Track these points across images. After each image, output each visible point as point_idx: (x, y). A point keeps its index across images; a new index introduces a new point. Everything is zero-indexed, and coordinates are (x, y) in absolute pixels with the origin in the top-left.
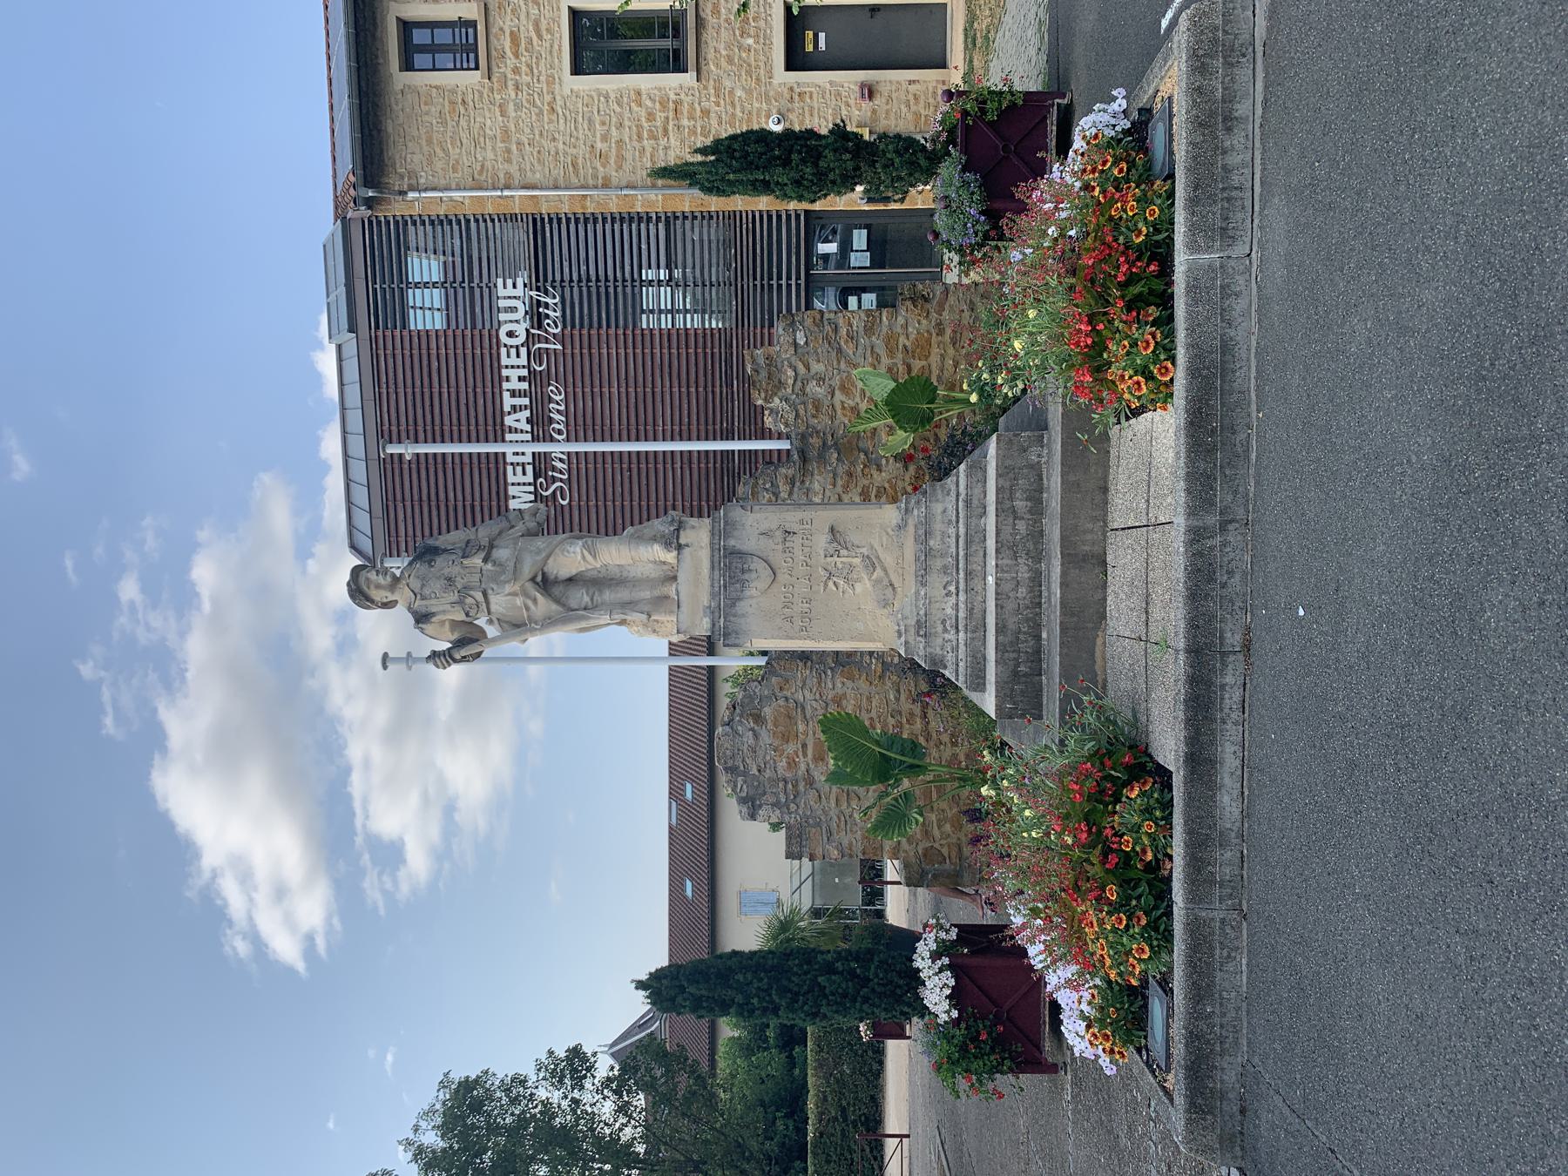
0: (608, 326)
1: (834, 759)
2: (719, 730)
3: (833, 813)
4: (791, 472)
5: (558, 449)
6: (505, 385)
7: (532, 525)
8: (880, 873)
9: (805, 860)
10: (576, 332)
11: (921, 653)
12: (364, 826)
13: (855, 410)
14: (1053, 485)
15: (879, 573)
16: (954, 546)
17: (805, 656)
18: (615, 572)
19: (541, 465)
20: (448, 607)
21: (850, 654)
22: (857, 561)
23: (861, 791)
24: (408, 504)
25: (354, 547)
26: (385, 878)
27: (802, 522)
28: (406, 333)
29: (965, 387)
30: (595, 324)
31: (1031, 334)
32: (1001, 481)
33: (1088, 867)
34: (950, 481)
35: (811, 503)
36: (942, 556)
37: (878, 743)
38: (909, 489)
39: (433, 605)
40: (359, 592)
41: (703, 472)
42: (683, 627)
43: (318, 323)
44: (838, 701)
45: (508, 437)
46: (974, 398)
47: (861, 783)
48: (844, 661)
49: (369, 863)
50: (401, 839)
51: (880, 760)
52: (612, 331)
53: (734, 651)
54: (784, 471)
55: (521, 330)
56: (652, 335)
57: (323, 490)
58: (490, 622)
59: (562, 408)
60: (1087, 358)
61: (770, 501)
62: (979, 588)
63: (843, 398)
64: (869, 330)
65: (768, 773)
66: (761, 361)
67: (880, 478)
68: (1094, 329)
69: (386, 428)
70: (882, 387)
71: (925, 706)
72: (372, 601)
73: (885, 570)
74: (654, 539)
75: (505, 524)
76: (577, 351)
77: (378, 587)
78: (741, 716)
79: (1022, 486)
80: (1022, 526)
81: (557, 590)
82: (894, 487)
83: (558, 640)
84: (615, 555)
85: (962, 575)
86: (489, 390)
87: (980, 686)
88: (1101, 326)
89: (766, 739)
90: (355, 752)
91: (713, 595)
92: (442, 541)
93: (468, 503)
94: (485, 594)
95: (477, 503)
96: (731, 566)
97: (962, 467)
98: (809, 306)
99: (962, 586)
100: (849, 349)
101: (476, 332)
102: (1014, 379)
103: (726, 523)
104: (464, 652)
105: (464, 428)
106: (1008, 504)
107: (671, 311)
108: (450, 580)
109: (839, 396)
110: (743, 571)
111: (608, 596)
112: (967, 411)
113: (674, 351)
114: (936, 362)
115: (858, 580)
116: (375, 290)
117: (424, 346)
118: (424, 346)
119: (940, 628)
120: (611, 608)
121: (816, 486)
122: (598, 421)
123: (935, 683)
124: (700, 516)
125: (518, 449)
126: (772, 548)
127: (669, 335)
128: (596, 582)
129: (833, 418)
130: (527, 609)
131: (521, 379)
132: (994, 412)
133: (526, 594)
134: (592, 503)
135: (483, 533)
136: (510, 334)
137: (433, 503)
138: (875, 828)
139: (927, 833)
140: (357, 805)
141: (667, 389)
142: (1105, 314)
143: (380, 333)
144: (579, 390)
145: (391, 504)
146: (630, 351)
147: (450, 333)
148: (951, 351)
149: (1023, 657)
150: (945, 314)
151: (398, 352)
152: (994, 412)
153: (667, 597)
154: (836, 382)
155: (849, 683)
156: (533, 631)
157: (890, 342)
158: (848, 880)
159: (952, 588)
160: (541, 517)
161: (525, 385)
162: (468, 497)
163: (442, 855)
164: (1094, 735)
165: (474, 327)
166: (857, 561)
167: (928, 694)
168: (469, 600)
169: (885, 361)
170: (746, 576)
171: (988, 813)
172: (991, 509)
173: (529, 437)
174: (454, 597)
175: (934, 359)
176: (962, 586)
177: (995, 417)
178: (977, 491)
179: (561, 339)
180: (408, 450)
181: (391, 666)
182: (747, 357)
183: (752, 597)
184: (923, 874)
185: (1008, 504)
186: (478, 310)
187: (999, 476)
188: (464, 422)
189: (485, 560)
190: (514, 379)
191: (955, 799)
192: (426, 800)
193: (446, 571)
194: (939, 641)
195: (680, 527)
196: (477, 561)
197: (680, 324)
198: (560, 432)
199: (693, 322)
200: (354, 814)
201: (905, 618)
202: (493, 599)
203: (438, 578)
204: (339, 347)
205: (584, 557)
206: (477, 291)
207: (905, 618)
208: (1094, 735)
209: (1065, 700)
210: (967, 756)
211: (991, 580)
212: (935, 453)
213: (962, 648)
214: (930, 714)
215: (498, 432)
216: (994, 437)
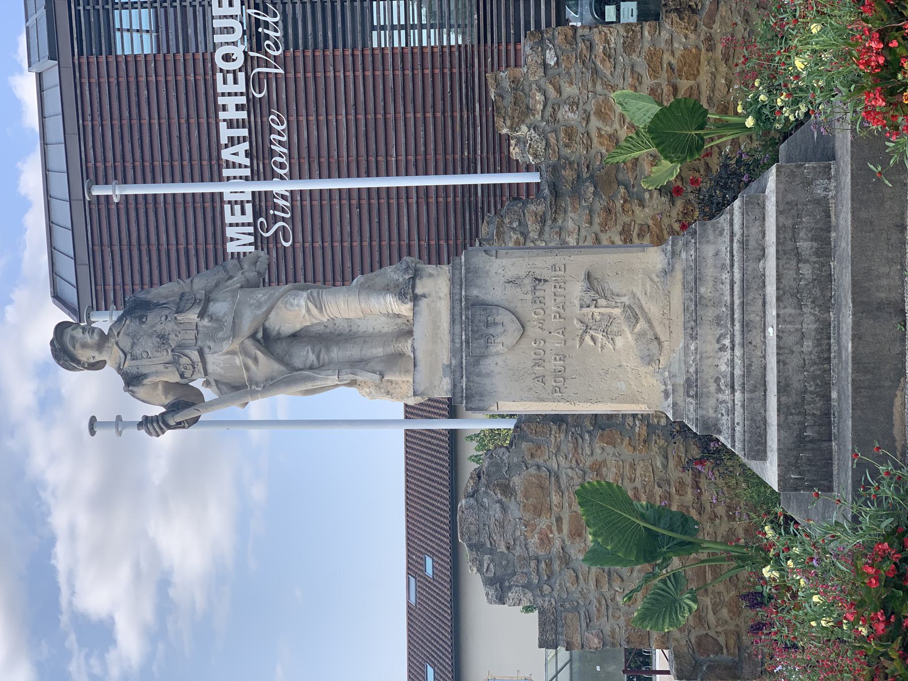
0: (335, 47)
1: (594, 534)
2: (463, 502)
3: (593, 596)
4: (540, 209)
5: (279, 187)
6: (222, 115)
7: (252, 275)
8: (647, 660)
9: (562, 650)
10: (299, 54)
11: (692, 416)
12: (70, 603)
13: (613, 138)
14: (842, 222)
15: (642, 325)
16: (728, 292)
17: (559, 420)
18: (343, 327)
19: (262, 204)
20: (161, 367)
21: (610, 417)
22: (617, 311)
23: (625, 571)
24: (116, 248)
25: (57, 297)
26: (94, 661)
27: (554, 267)
28: (112, 59)
29: (740, 109)
30: (321, 45)
31: (814, 52)
32: (781, 219)
33: (887, 663)
34: (723, 220)
35: (563, 246)
36: (714, 305)
37: (643, 517)
38: (677, 226)
39: (144, 366)
40: (64, 350)
41: (442, 207)
42: (421, 388)
43: (16, 45)
44: (597, 468)
45: (226, 172)
46: (750, 122)
47: (621, 562)
48: (603, 424)
49: (75, 646)
51: (647, 536)
52: (339, 52)
53: (479, 415)
54: (532, 207)
55: (238, 52)
56: (383, 55)
57: (22, 230)
58: (207, 384)
59: (285, 139)
60: (879, 79)
61: (517, 243)
62: (757, 340)
63: (600, 124)
64: (629, 46)
65: (518, 551)
66: (506, 84)
67: (642, 215)
68: (886, 46)
69: (91, 164)
70: (644, 111)
71: (697, 475)
72: (78, 362)
73: (649, 321)
74: (386, 289)
75: (222, 275)
76: (300, 75)
77: (84, 346)
78: (487, 486)
79: (807, 223)
80: (806, 270)
81: (280, 348)
82: (659, 225)
83: (282, 403)
84: (344, 307)
85: (737, 326)
86: (203, 121)
87: (760, 454)
88: (894, 44)
89: (515, 511)
90: (59, 520)
91: (454, 352)
92: (156, 293)
93: (182, 247)
95: (192, 247)
96: (474, 320)
97: (737, 203)
98: (562, 21)
99: (738, 339)
100: (606, 69)
101: (189, 57)
102: (796, 102)
103: (468, 271)
104: (179, 418)
105: (177, 164)
106: (789, 245)
107: (404, 27)
108: (163, 338)
109: (595, 122)
110: (488, 325)
111: (336, 353)
112: (742, 137)
113: (409, 72)
114: (707, 81)
115: (620, 333)
116: (78, 12)
117: (132, 73)
118: (132, 73)
119: (713, 388)
120: (339, 367)
121: (570, 224)
122: (324, 153)
123: (708, 450)
124: (439, 262)
125: (236, 189)
126: (520, 297)
127: (403, 54)
128: (322, 338)
129: (588, 147)
130: (247, 369)
131: (239, 108)
132: (774, 138)
133: (246, 353)
134: (318, 244)
135: (200, 284)
136: (227, 58)
137: (144, 248)
138: (643, 617)
139: (700, 617)
140: (62, 579)
141: (401, 116)
142: (899, 29)
143: (84, 60)
144: (303, 119)
145: (97, 248)
146: (359, 73)
147: (161, 58)
148: (723, 69)
149: (809, 421)
150: (716, 26)
151: (104, 80)
152: (774, 138)
153: (401, 355)
154: (592, 106)
155: (610, 449)
156: (254, 394)
157: (654, 60)
158: (612, 668)
159: (727, 342)
160: (262, 265)
161: (243, 115)
162: (182, 240)
163: (156, 634)
164: (892, 510)
165: (186, 50)
166: (617, 311)
167: (701, 461)
168: (184, 360)
169: (648, 81)
170: (491, 330)
171: (770, 598)
172: (771, 251)
173: (247, 172)
174: (169, 357)
175: (704, 79)
176: (738, 339)
177: (775, 144)
178: (754, 231)
179: (282, 62)
180: (116, 192)
181: (99, 432)
182: (490, 81)
183: (498, 354)
184: (697, 666)
185: (789, 245)
186: (191, 31)
187: (779, 212)
188: (176, 155)
189: (201, 315)
190: (231, 108)
191: (733, 581)
192: (138, 575)
193: (159, 328)
194: (712, 402)
195: (416, 275)
196: (192, 316)
197: (414, 42)
198: (282, 166)
199: (429, 38)
200: (58, 590)
201: (672, 376)
202: (210, 358)
203: (150, 336)
204: (40, 76)
205: (308, 310)
206: (190, 11)
207: (672, 376)
208: (892, 510)
209: (860, 469)
210: (746, 531)
211: (771, 332)
212: (705, 186)
213: (739, 410)
214: (703, 483)
215: (214, 169)
216: (774, 169)
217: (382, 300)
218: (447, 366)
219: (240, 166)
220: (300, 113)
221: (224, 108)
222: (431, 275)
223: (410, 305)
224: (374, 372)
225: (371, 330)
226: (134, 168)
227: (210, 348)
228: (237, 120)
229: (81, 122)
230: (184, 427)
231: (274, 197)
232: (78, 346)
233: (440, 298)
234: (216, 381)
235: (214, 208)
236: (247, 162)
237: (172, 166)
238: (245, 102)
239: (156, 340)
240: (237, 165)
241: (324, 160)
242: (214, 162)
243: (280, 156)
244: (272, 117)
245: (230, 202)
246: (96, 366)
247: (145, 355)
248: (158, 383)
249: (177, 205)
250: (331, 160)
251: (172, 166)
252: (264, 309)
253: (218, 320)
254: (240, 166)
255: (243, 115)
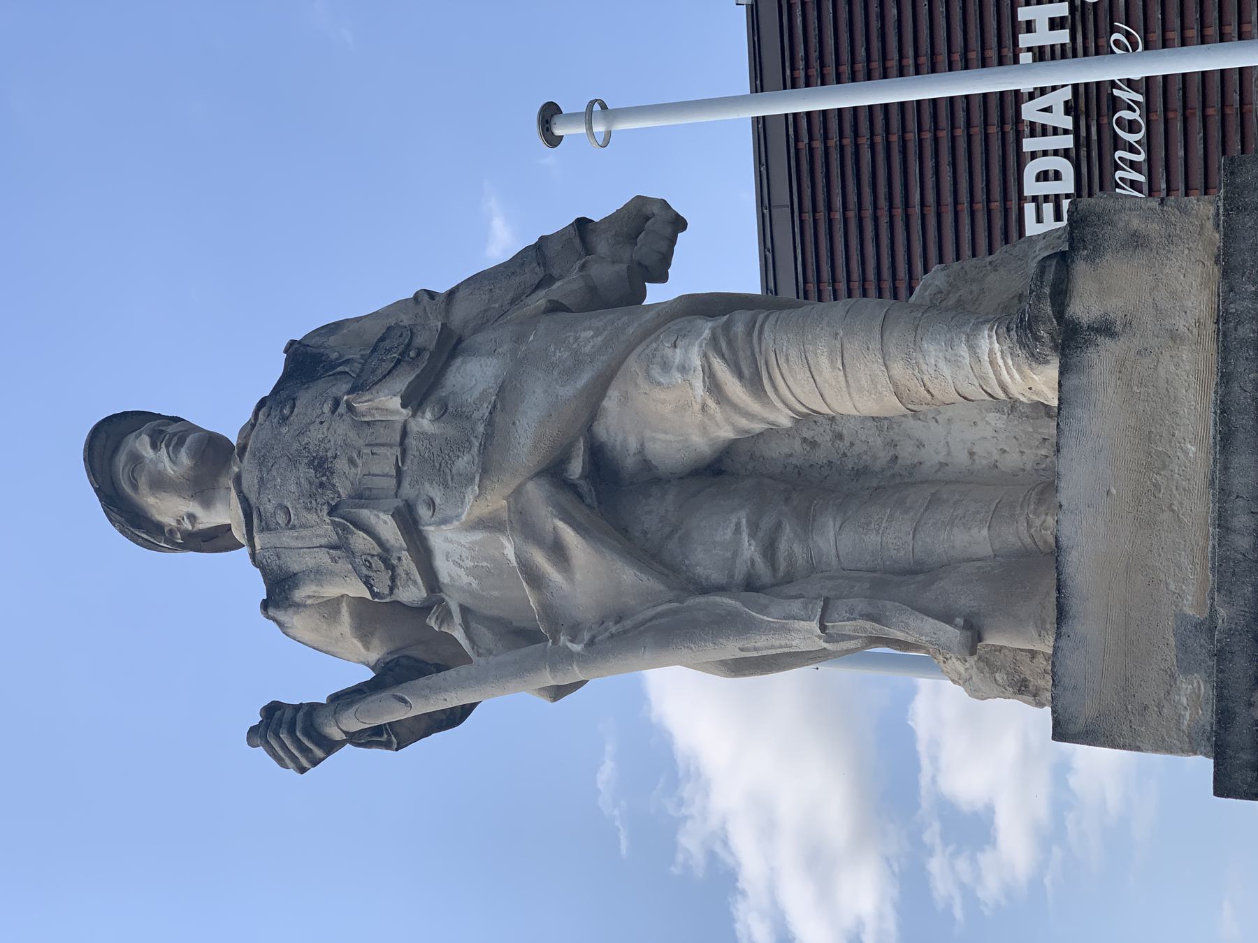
6: (1025, 40)
50: (990, 810)
77: (160, 484)
81: (652, 515)
91: (1225, 571)
94: (408, 521)
105: (944, 135)
111: (834, 540)
130: (535, 579)
131: (1055, 24)
133: (527, 529)
140: (922, 748)
161: (1063, 36)
163: (1051, 837)
189: (414, 399)
196: (387, 402)
198: (1132, 127)
200: (917, 768)
203: (293, 462)
205: (714, 387)
217: (963, 350)
218: (1198, 626)
219: (1055, 131)
220: (1169, 26)
221: (1030, 27)
222: (1136, 242)
223: (1051, 372)
224: (948, 618)
225: (961, 458)
226: (873, 146)
227: (431, 504)
228: (1052, 46)
229: (788, 72)
230: (387, 745)
231: (1118, 186)
232: (143, 481)
233: (1174, 336)
234: (464, 610)
235: (1006, 211)
236: (1068, 122)
237: (936, 140)
238: (1066, 13)
239: (306, 473)
240: (1050, 130)
241: (1213, 112)
242: (1008, 128)
243: (1130, 109)
244: (1116, 36)
245: (1035, 199)
246: (213, 540)
247: (281, 519)
248: (338, 600)
249: (943, 209)
250: (1228, 111)
251: (936, 140)
252: (585, 378)
253: (459, 415)
254: (1055, 131)
255: (1063, 36)
